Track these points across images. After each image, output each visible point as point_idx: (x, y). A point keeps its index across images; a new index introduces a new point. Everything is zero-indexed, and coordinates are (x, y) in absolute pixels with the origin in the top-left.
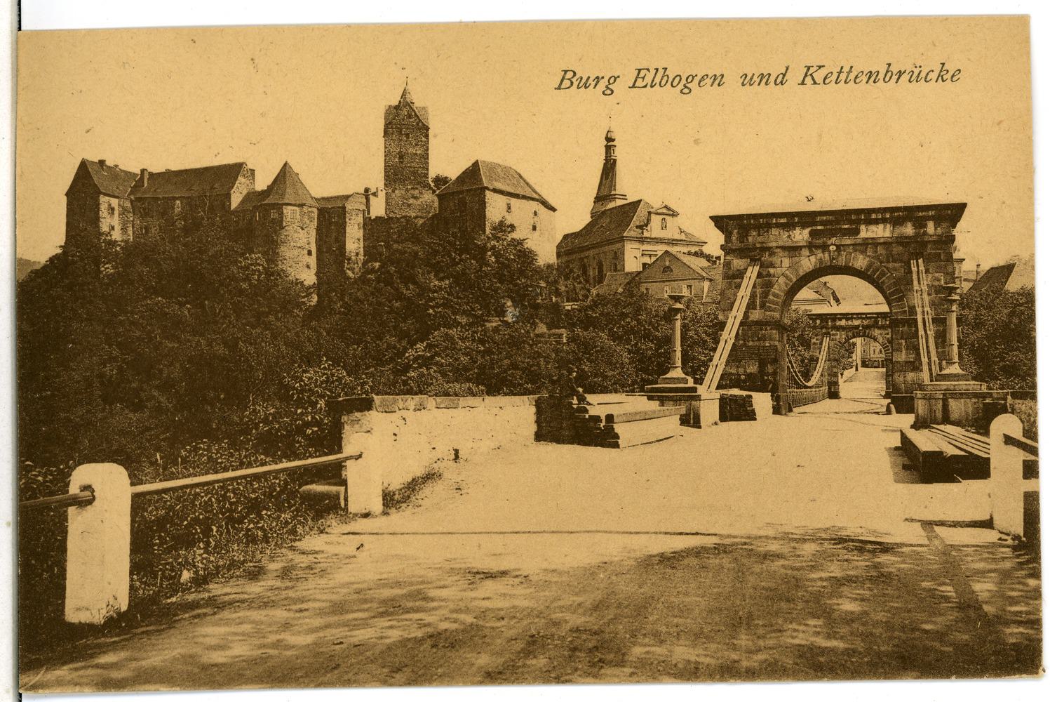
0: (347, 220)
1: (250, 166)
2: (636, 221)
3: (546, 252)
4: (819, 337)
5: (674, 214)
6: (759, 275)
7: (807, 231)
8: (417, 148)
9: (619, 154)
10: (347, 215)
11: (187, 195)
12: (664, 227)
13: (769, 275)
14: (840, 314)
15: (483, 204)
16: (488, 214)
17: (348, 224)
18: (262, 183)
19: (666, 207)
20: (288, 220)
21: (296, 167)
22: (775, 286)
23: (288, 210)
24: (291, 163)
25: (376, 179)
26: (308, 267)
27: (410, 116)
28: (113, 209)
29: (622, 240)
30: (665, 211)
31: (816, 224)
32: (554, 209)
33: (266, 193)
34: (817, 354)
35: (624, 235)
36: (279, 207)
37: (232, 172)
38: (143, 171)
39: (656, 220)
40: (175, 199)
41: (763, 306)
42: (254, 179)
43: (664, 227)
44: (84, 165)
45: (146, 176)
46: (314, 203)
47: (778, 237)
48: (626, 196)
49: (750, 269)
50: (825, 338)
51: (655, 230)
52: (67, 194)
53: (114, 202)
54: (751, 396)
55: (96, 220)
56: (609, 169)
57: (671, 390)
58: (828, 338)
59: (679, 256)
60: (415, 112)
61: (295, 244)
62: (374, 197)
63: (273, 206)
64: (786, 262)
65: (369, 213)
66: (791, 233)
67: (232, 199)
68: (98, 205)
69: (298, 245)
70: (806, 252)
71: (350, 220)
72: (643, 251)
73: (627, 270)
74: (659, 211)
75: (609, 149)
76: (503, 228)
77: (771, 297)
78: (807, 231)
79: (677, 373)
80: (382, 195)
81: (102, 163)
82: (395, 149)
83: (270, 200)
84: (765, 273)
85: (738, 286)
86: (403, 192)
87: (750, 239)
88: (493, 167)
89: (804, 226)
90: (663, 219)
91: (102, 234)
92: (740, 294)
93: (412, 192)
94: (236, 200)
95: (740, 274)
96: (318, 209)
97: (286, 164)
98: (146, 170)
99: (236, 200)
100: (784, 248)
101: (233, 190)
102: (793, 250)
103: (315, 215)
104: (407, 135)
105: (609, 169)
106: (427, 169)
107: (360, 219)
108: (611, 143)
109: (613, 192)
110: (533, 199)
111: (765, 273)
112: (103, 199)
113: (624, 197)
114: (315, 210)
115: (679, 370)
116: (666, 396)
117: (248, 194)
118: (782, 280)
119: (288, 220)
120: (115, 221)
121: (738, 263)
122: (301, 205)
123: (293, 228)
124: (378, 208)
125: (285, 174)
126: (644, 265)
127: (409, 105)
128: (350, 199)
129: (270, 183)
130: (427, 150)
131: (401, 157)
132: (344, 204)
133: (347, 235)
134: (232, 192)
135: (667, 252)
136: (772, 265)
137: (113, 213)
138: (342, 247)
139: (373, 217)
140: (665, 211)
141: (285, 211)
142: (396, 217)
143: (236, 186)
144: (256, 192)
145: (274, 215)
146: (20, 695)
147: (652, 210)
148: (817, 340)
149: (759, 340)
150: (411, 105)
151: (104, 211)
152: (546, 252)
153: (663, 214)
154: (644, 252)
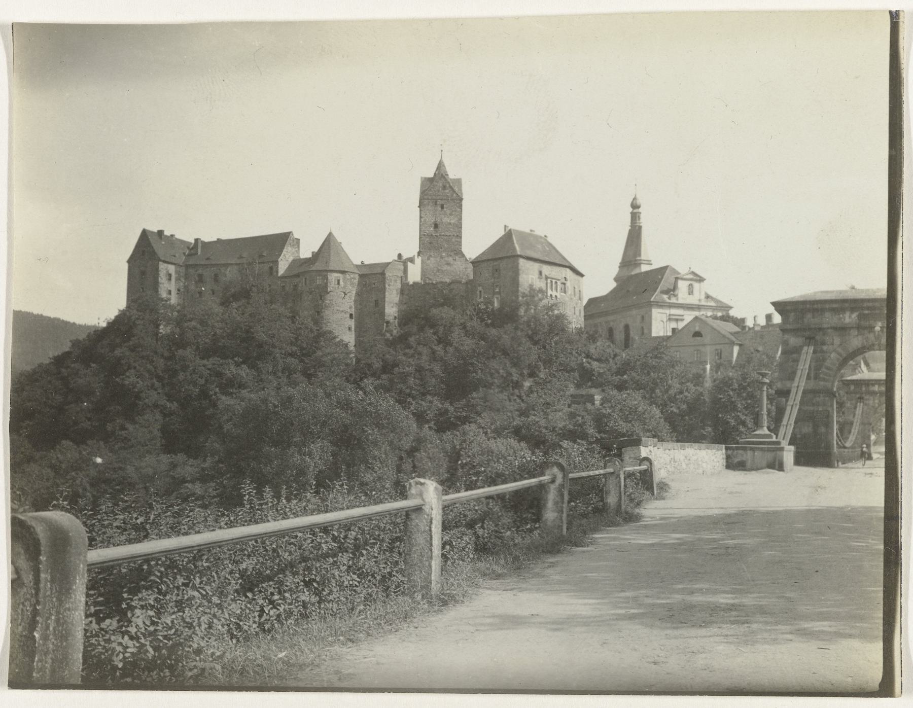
0: (387, 286)
1: (296, 236)
2: (663, 286)
3: (576, 320)
4: (854, 402)
5: (701, 280)
6: (814, 352)
7: (855, 315)
8: (452, 217)
9: (645, 222)
10: (387, 281)
11: (238, 262)
12: (691, 292)
13: (822, 351)
14: (872, 380)
15: (516, 272)
16: (521, 279)
17: (387, 290)
18: (305, 252)
19: (693, 273)
20: (332, 285)
21: (339, 237)
22: (828, 361)
23: (333, 277)
24: (335, 234)
25: (411, 247)
26: (350, 329)
27: (444, 188)
28: (170, 275)
29: (650, 305)
30: (691, 276)
31: (863, 308)
32: (582, 275)
33: (307, 261)
34: (851, 418)
35: (652, 300)
36: (324, 273)
37: (281, 240)
38: (197, 240)
39: (683, 286)
40: (226, 265)
41: (815, 378)
42: (299, 247)
43: (691, 292)
44: (145, 234)
45: (200, 245)
46: (356, 271)
47: (829, 320)
48: (650, 261)
49: (805, 348)
50: (859, 404)
51: (683, 296)
52: (129, 261)
53: (172, 269)
54: (658, 484)
55: (156, 285)
56: (634, 237)
57: (753, 443)
58: (862, 404)
59: (710, 321)
60: (449, 184)
61: (338, 308)
62: (412, 264)
63: (319, 272)
64: (837, 341)
65: (406, 277)
66: (841, 316)
67: (280, 266)
68: (157, 270)
69: (341, 309)
70: (854, 332)
71: (389, 285)
72: (670, 315)
73: (654, 334)
74: (685, 277)
75: (635, 217)
76: (533, 292)
77: (824, 370)
78: (855, 315)
79: (765, 431)
80: (418, 261)
81: (160, 233)
82: (430, 220)
83: (318, 266)
84: (819, 349)
85: (797, 361)
86: (438, 259)
87: (806, 320)
88: (523, 236)
89: (852, 310)
90: (690, 285)
91: (162, 300)
92: (800, 367)
93: (446, 259)
94: (283, 267)
95: (797, 350)
96: (359, 275)
97: (330, 234)
98: (200, 239)
99: (283, 267)
100: (835, 329)
101: (281, 257)
102: (842, 329)
103: (356, 281)
104: (442, 207)
105: (634, 237)
106: (461, 237)
107: (399, 285)
108: (635, 211)
109: (638, 258)
110: (566, 266)
111: (819, 349)
112: (162, 266)
113: (649, 263)
114: (357, 276)
115: (765, 428)
116: (756, 448)
117: (294, 261)
118: (833, 355)
119: (332, 285)
120: (173, 286)
121: (794, 341)
122: (343, 272)
123: (337, 293)
124: (415, 274)
125: (329, 243)
126: (674, 330)
127: (444, 177)
128: (390, 266)
129: (316, 250)
130: (461, 219)
131: (436, 226)
132: (384, 271)
133: (386, 299)
134: (279, 260)
135: (696, 318)
136: (823, 343)
137: (170, 279)
138: (382, 314)
139: (411, 283)
140: (691, 276)
141: (330, 278)
142: (432, 283)
143: (283, 254)
144: (301, 259)
145: (319, 281)
146: (646, 526)
147: (679, 276)
148: (851, 404)
149: (813, 405)
150: (446, 176)
151: (163, 279)
152: (576, 320)
153: (691, 280)
154: (672, 317)
